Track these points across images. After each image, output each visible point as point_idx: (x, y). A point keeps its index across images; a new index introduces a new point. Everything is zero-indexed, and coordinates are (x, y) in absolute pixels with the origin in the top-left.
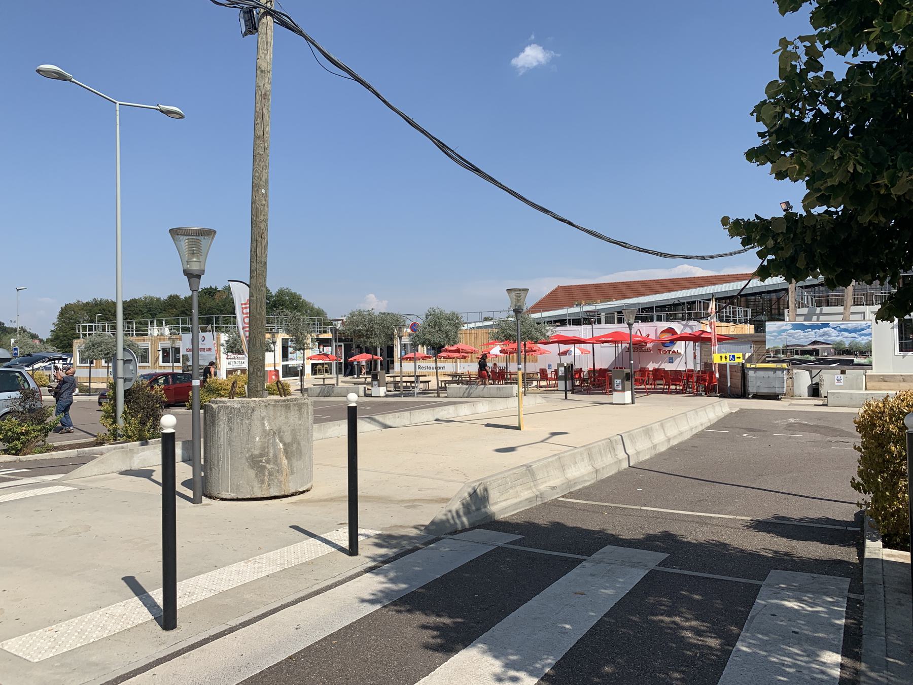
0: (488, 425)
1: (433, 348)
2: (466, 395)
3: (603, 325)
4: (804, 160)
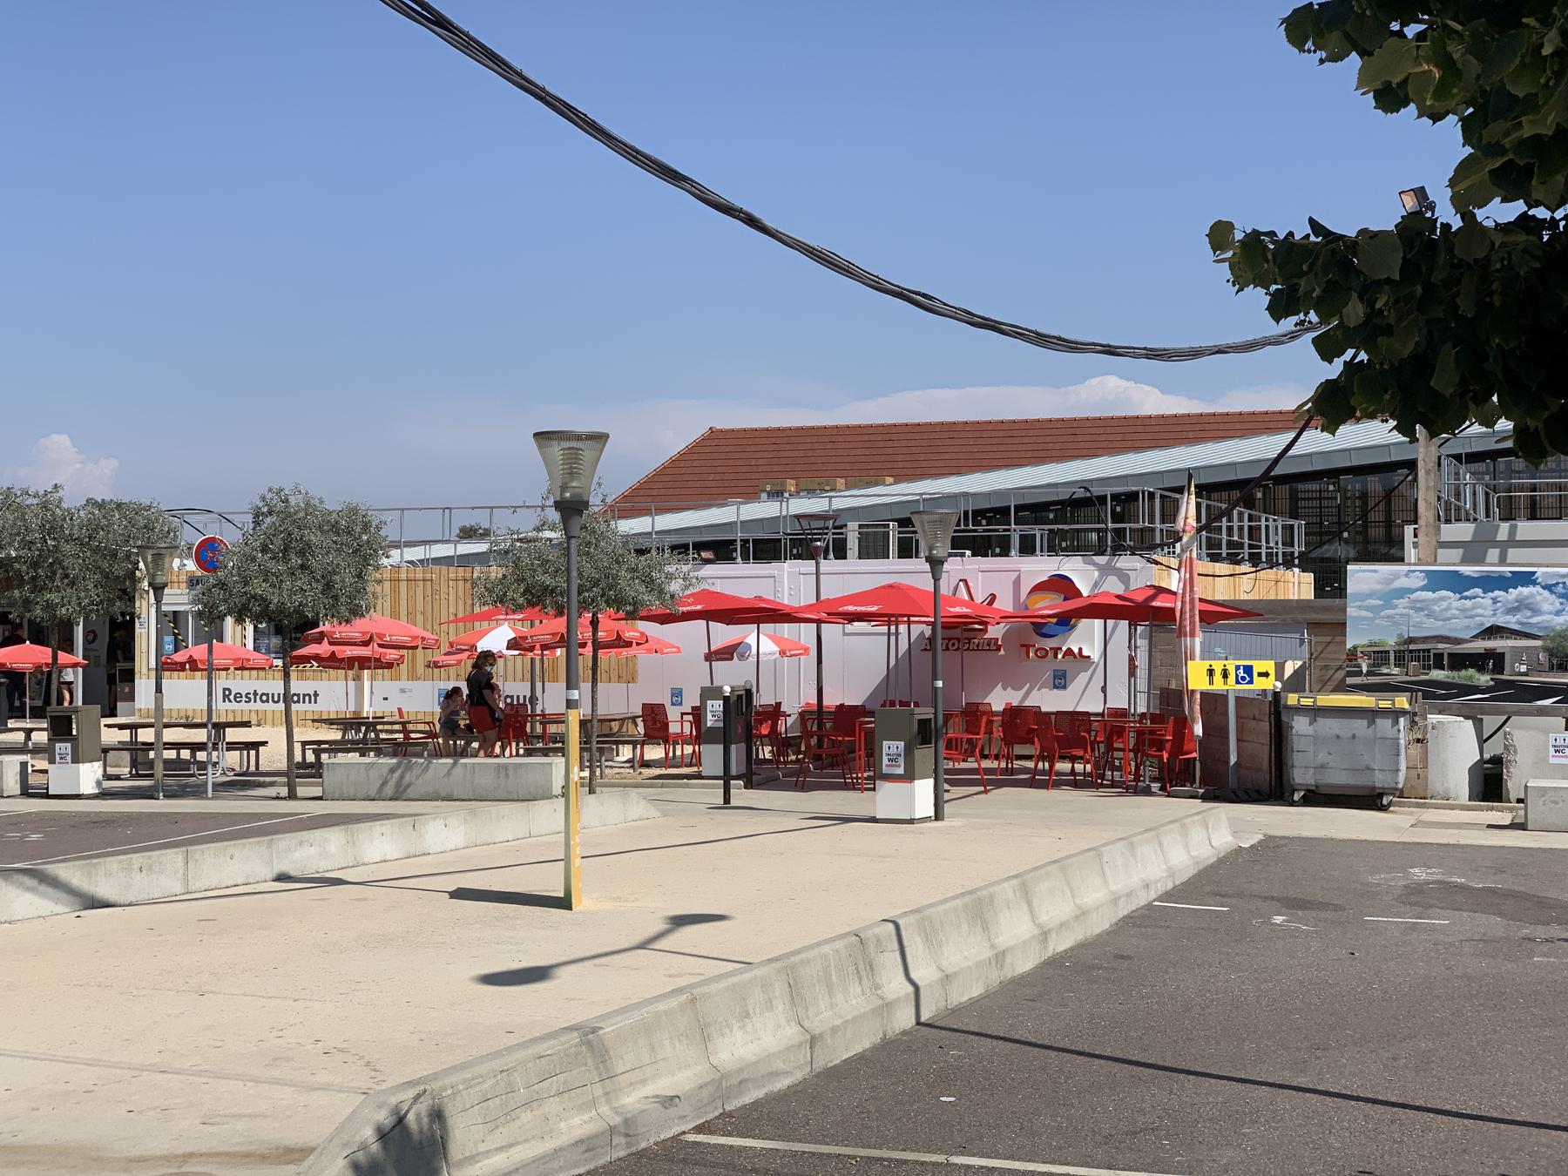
0: (459, 894)
1: (279, 631)
2: (389, 790)
3: (853, 563)
4: (1456, 51)
